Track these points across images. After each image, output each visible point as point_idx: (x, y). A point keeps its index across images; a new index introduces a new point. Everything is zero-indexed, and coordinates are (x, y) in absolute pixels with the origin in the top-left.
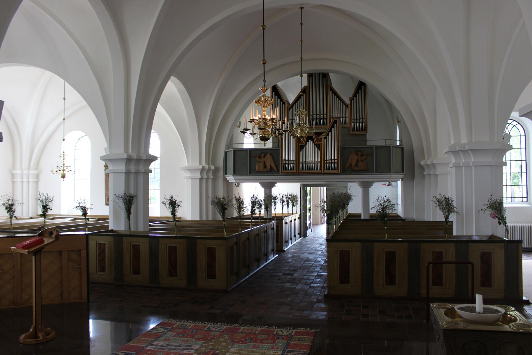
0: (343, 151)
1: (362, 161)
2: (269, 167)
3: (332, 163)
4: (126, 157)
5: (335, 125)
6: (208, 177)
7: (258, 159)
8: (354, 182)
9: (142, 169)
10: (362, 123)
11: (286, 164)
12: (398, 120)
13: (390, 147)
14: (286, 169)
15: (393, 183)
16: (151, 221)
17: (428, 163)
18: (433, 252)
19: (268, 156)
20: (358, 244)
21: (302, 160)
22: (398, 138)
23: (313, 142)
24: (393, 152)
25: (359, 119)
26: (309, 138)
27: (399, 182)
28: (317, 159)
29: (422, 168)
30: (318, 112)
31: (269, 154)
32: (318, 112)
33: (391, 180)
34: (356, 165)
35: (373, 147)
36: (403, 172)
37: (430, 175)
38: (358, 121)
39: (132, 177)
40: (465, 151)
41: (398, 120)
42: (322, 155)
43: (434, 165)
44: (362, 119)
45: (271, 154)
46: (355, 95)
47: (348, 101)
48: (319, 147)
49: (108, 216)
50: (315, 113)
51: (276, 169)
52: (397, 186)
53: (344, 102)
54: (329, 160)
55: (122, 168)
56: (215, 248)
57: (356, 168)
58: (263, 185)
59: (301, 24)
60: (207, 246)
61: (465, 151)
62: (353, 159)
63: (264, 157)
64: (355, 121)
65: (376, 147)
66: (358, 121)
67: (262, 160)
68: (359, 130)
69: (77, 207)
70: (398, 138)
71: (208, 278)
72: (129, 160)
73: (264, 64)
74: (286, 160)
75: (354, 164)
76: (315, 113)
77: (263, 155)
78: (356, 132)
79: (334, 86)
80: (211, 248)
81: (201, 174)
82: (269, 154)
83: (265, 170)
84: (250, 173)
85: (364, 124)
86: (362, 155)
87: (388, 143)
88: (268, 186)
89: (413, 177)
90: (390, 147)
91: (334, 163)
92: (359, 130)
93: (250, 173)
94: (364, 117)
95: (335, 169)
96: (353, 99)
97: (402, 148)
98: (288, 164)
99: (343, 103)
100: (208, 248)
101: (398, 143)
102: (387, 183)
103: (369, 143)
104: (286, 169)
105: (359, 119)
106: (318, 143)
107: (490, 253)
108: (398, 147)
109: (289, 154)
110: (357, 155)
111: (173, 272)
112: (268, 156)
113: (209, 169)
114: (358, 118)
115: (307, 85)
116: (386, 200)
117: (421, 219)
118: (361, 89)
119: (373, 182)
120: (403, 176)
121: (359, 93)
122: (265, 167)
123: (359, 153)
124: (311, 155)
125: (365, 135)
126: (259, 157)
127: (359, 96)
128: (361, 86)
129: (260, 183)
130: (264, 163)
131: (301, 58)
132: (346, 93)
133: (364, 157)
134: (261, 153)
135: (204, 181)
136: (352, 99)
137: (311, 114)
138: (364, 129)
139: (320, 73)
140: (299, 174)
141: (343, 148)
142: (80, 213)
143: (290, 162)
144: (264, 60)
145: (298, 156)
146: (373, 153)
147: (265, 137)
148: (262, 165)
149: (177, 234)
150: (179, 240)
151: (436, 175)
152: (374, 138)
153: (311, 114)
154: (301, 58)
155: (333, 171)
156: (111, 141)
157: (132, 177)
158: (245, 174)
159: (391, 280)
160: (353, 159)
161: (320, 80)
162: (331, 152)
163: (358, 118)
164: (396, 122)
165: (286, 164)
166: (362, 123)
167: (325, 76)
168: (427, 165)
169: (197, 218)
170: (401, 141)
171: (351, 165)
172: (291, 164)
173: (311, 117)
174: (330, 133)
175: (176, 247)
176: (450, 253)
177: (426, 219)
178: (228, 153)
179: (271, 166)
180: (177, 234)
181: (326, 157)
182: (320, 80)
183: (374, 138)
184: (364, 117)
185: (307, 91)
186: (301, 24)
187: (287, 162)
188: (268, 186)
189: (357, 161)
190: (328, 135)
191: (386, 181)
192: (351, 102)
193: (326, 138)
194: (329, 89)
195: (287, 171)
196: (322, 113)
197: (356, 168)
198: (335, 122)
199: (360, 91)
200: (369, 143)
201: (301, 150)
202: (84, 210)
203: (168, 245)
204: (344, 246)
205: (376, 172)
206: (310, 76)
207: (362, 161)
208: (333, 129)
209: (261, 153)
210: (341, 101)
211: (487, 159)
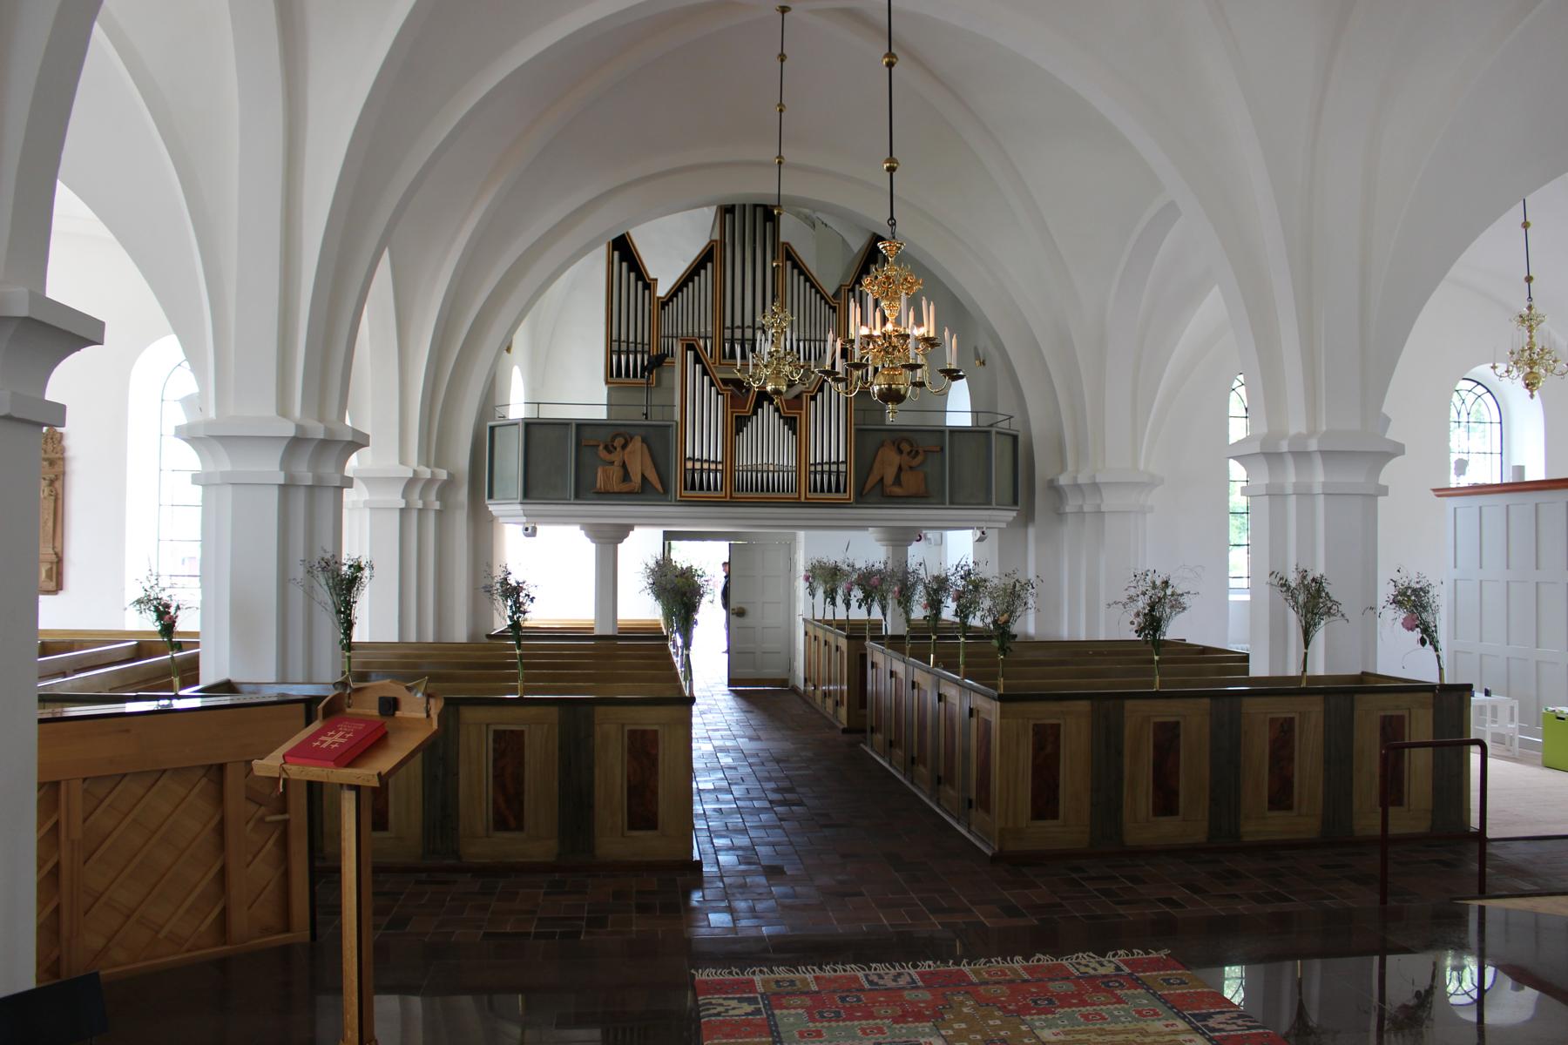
2: (636, 479)
3: (830, 472)
4: (292, 434)
6: (425, 503)
7: (602, 452)
8: (864, 528)
9: (328, 470)
11: (694, 470)
12: (977, 356)
14: (693, 488)
15: (930, 534)
16: (46, 649)
17: (1080, 481)
18: (1272, 720)
19: (637, 445)
20: (1084, 706)
21: (743, 460)
23: (777, 410)
28: (787, 459)
29: (1054, 489)
31: (638, 440)
34: (898, 481)
36: (1015, 503)
37: (1080, 513)
39: (299, 500)
40: (1301, 456)
41: (977, 356)
42: (801, 450)
43: (1096, 487)
45: (644, 441)
48: (791, 423)
49: (196, 634)
51: (659, 487)
54: (822, 464)
55: (270, 468)
56: (655, 732)
57: (897, 490)
59: (782, 57)
60: (627, 728)
61: (1301, 456)
62: (889, 463)
63: (624, 447)
67: (616, 457)
69: (139, 602)
71: (633, 826)
72: (296, 443)
73: (891, 170)
74: (693, 459)
75: (889, 479)
76: (738, 322)
77: (619, 442)
80: (644, 732)
81: (405, 495)
82: (638, 440)
83: (625, 487)
84: (577, 496)
86: (914, 453)
90: (988, 433)
91: (838, 472)
93: (577, 496)
95: (838, 490)
98: (702, 470)
100: (632, 733)
104: (693, 488)
107: (1401, 719)
109: (703, 440)
110: (900, 451)
111: (508, 814)
112: (637, 445)
113: (429, 482)
116: (1158, 583)
117: (1051, 636)
119: (630, 527)
122: (626, 477)
123: (906, 447)
126: (606, 448)
129: (584, 527)
130: (624, 465)
131: (780, 156)
133: (920, 458)
135: (414, 516)
137: (728, 323)
139: (755, 206)
140: (733, 503)
142: (148, 623)
143: (706, 466)
144: (891, 159)
145: (730, 450)
146: (942, 449)
147: (898, 391)
148: (616, 472)
149: (526, 690)
150: (533, 711)
151: (1099, 513)
153: (728, 323)
154: (780, 156)
155: (833, 495)
156: (223, 375)
157: (299, 500)
158: (559, 499)
159: (1166, 801)
162: (830, 442)
165: (694, 470)
167: (768, 214)
168: (1077, 487)
169: (396, 640)
173: (728, 334)
175: (522, 732)
176: (1194, 719)
177: (1065, 634)
178: (497, 431)
180: (526, 690)
185: (717, 254)
186: (782, 57)
187: (698, 465)
189: (900, 469)
193: (814, 398)
197: (897, 490)
201: (739, 430)
202: (165, 614)
203: (492, 728)
204: (1045, 713)
206: (727, 211)
211: (1353, 478)
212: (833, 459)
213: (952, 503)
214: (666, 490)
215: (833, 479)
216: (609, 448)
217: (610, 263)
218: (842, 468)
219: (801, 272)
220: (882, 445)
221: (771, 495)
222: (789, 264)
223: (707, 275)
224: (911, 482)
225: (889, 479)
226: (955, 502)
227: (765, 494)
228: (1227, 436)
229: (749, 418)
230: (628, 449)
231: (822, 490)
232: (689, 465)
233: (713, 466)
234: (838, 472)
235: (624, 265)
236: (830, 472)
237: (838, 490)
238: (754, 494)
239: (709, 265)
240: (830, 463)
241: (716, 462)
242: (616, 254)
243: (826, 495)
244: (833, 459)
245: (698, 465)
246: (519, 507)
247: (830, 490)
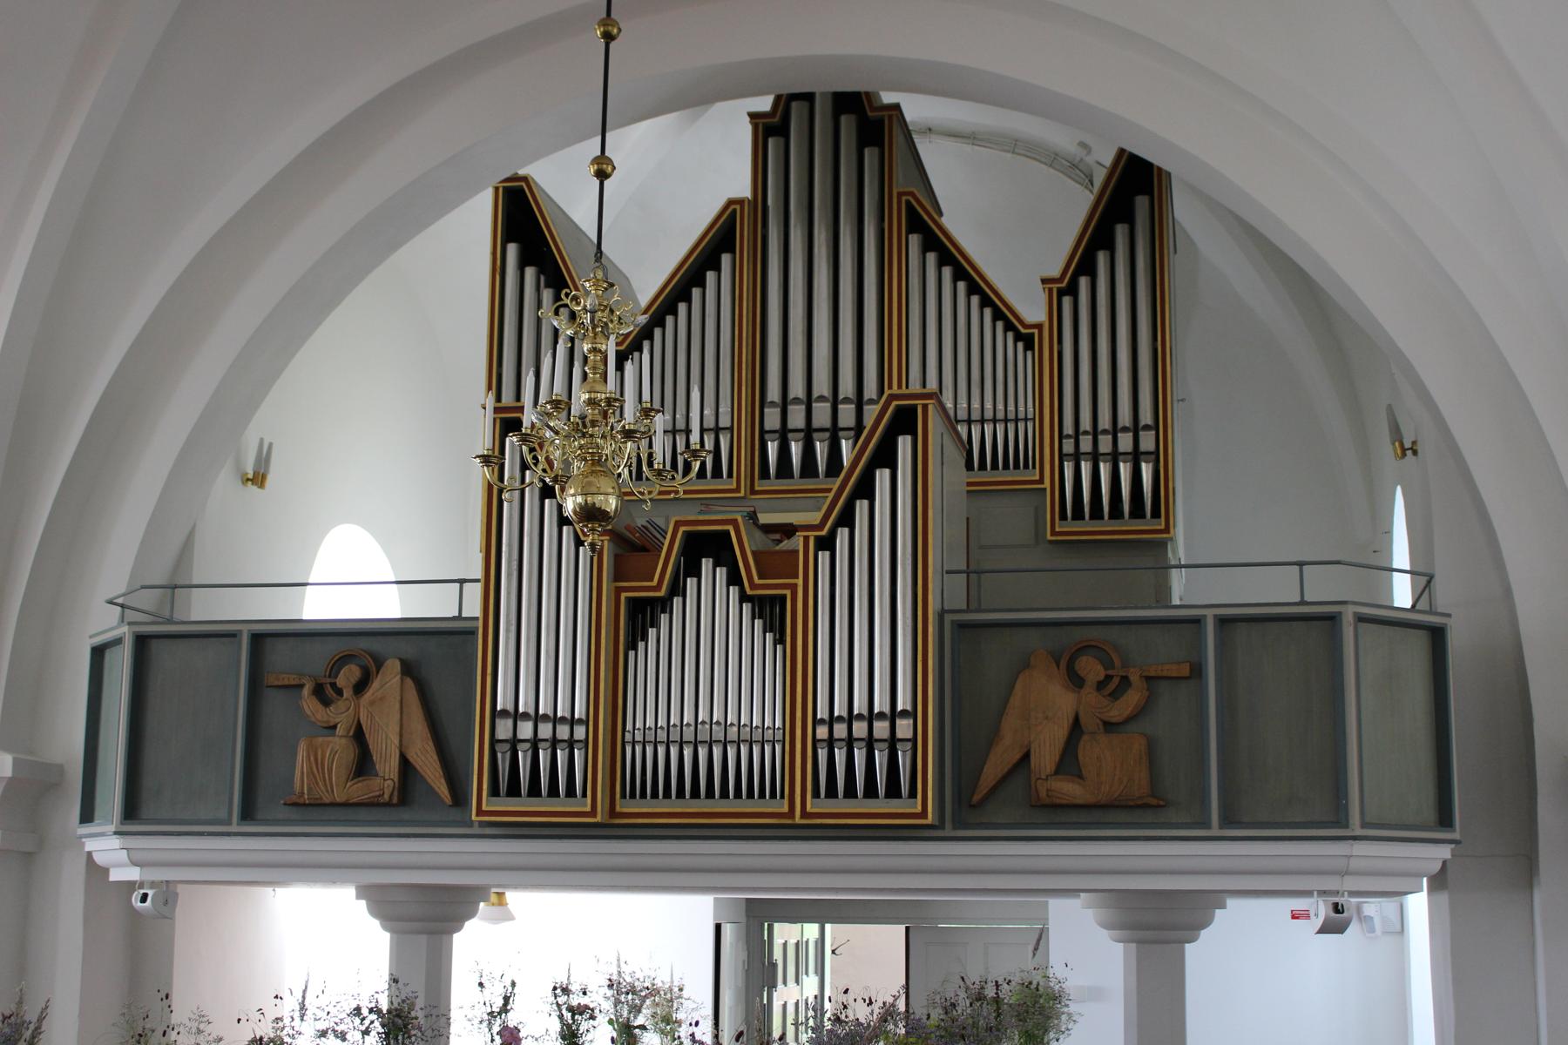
0: (966, 648)
1: (1109, 726)
2: (387, 767)
3: (850, 741)
5: (904, 443)
7: (309, 704)
10: (1136, 457)
11: (514, 742)
12: (1396, 433)
13: (1332, 619)
14: (514, 790)
15: (1372, 907)
19: (390, 680)
21: (645, 715)
22: (1401, 556)
23: (734, 579)
24: (1363, 660)
25: (1115, 431)
26: (706, 546)
27: (1418, 905)
30: (822, 386)
31: (393, 667)
32: (822, 386)
33: (1351, 883)
34: (1068, 762)
35: (1197, 621)
36: (1445, 818)
38: (1105, 444)
41: (1396, 433)
42: (797, 684)
44: (1136, 429)
45: (408, 669)
46: (1083, 264)
47: (1032, 308)
48: (771, 613)
50: (797, 389)
51: (442, 789)
52: (1402, 930)
53: (1002, 315)
57: (1069, 789)
58: (383, 902)
62: (1044, 711)
63: (360, 687)
64: (1086, 444)
65: (1224, 622)
66: (1105, 444)
67: (341, 714)
68: (1116, 512)
70: (1401, 556)
74: (517, 716)
75: (1046, 757)
76: (797, 389)
77: (348, 676)
78: (1087, 525)
79: (960, 221)
83: (358, 790)
84: (248, 812)
85: (1146, 471)
86: (1113, 686)
87: (1323, 588)
88: (425, 922)
89: (1520, 860)
90: (1332, 619)
91: (870, 742)
92: (1116, 512)
94: (1146, 417)
96: (1072, 290)
97: (1437, 636)
98: (535, 743)
99: (998, 315)
101: (1402, 594)
102: (1320, 910)
103: (1182, 589)
105: (1115, 431)
106: (769, 587)
108: (1397, 622)
110: (1075, 680)
112: (390, 680)
114: (1105, 422)
115: (742, 187)
118: (1130, 220)
119: (1215, 899)
120: (1445, 852)
121: (1110, 247)
122: (363, 765)
123: (1091, 669)
124: (714, 677)
125: (1157, 546)
126: (318, 691)
127: (1113, 268)
128: (1132, 193)
129: (364, 892)
130: (359, 736)
132: (1013, 227)
133: (1132, 698)
134: (345, 659)
136: (1063, 289)
137: (774, 393)
138: (1152, 506)
140: (613, 828)
141: (961, 626)
143: (545, 731)
145: (613, 691)
146: (1197, 671)
148: (339, 749)
152: (1226, 546)
153: (774, 393)
155: (881, 805)
158: (212, 826)
160: (1044, 711)
161: (838, 146)
162: (872, 660)
163: (1105, 422)
164: (1387, 449)
165: (514, 742)
166: (1136, 457)
170: (1424, 580)
171: (1026, 757)
172: (554, 742)
173: (772, 419)
174: (861, 506)
179: (405, 763)
181: (831, 698)
182: (838, 146)
183: (1226, 546)
184: (1146, 417)
187: (525, 730)
188: (425, 922)
189: (1076, 727)
190: (847, 519)
191: (1307, 894)
192: (1055, 312)
193: (827, 543)
194: (898, 220)
195: (523, 804)
196: (847, 387)
197: (1069, 789)
198: (905, 420)
199: (1121, 231)
200: (1182, 589)
201: (637, 635)
205: (1230, 819)
207: (1109, 726)
208: (882, 476)
209: (345, 659)
210: (974, 288)
212: (859, 706)
213: (1228, 820)
214: (459, 798)
215: (880, 758)
216: (321, 694)
217: (499, 270)
218: (904, 728)
219: (960, 274)
220: (1025, 665)
221: (718, 806)
222: (915, 240)
223: (720, 284)
224: (1110, 764)
225: (1046, 757)
226: (1239, 816)
227: (703, 805)
228: (536, 156)
229: (664, 604)
230: (368, 695)
231: (534, 791)
232: (504, 729)
233: (563, 732)
234: (893, 741)
235: (530, 272)
236: (850, 741)
237: (893, 791)
238: (674, 806)
239: (726, 259)
240: (871, 717)
241: (572, 722)
242: (512, 249)
243: (861, 805)
244: (859, 706)
245: (525, 730)
246: (116, 842)
247: (870, 791)
